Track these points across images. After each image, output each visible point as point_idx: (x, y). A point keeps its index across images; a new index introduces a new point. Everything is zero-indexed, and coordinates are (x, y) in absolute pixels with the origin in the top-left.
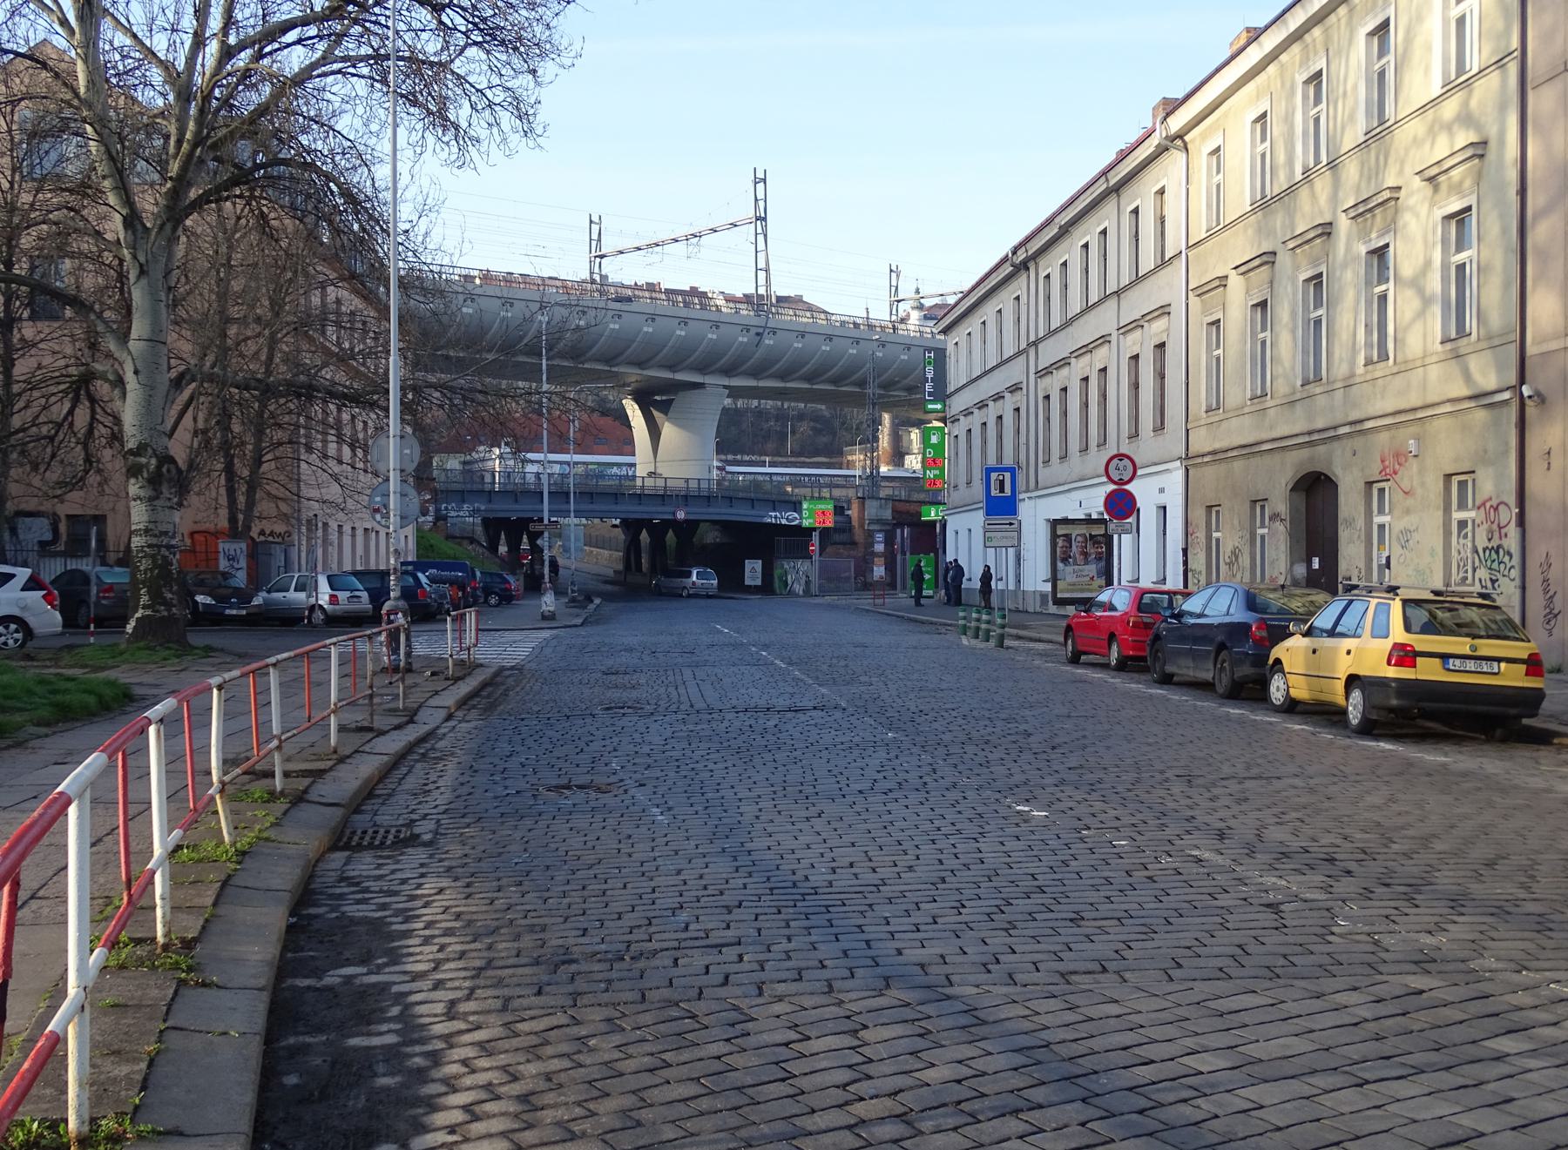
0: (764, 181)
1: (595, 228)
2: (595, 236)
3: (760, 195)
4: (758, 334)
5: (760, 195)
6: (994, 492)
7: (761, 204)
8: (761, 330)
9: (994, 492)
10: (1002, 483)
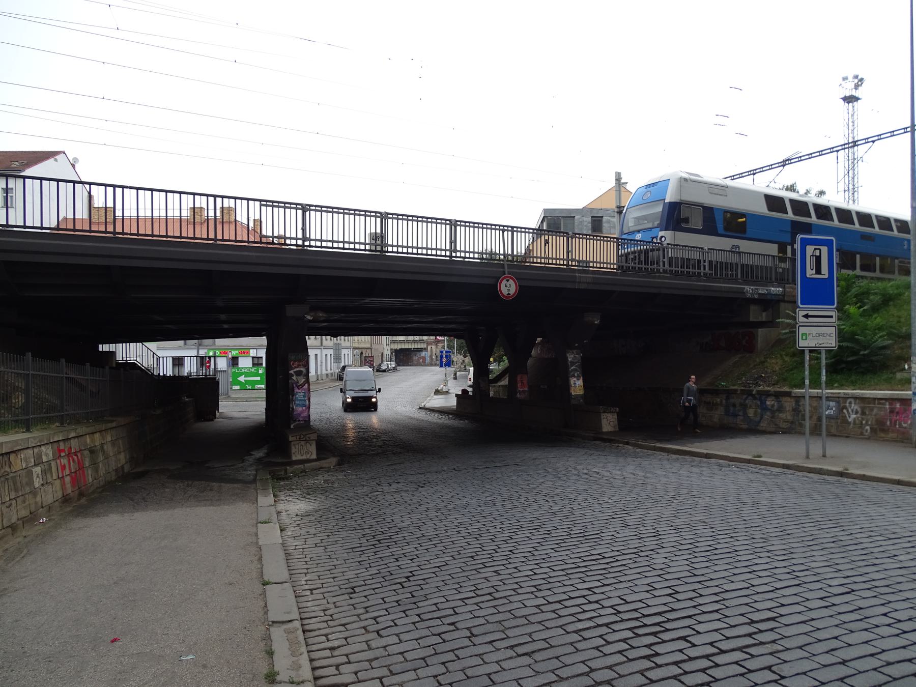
6: (810, 273)
9: (810, 273)
10: (818, 259)
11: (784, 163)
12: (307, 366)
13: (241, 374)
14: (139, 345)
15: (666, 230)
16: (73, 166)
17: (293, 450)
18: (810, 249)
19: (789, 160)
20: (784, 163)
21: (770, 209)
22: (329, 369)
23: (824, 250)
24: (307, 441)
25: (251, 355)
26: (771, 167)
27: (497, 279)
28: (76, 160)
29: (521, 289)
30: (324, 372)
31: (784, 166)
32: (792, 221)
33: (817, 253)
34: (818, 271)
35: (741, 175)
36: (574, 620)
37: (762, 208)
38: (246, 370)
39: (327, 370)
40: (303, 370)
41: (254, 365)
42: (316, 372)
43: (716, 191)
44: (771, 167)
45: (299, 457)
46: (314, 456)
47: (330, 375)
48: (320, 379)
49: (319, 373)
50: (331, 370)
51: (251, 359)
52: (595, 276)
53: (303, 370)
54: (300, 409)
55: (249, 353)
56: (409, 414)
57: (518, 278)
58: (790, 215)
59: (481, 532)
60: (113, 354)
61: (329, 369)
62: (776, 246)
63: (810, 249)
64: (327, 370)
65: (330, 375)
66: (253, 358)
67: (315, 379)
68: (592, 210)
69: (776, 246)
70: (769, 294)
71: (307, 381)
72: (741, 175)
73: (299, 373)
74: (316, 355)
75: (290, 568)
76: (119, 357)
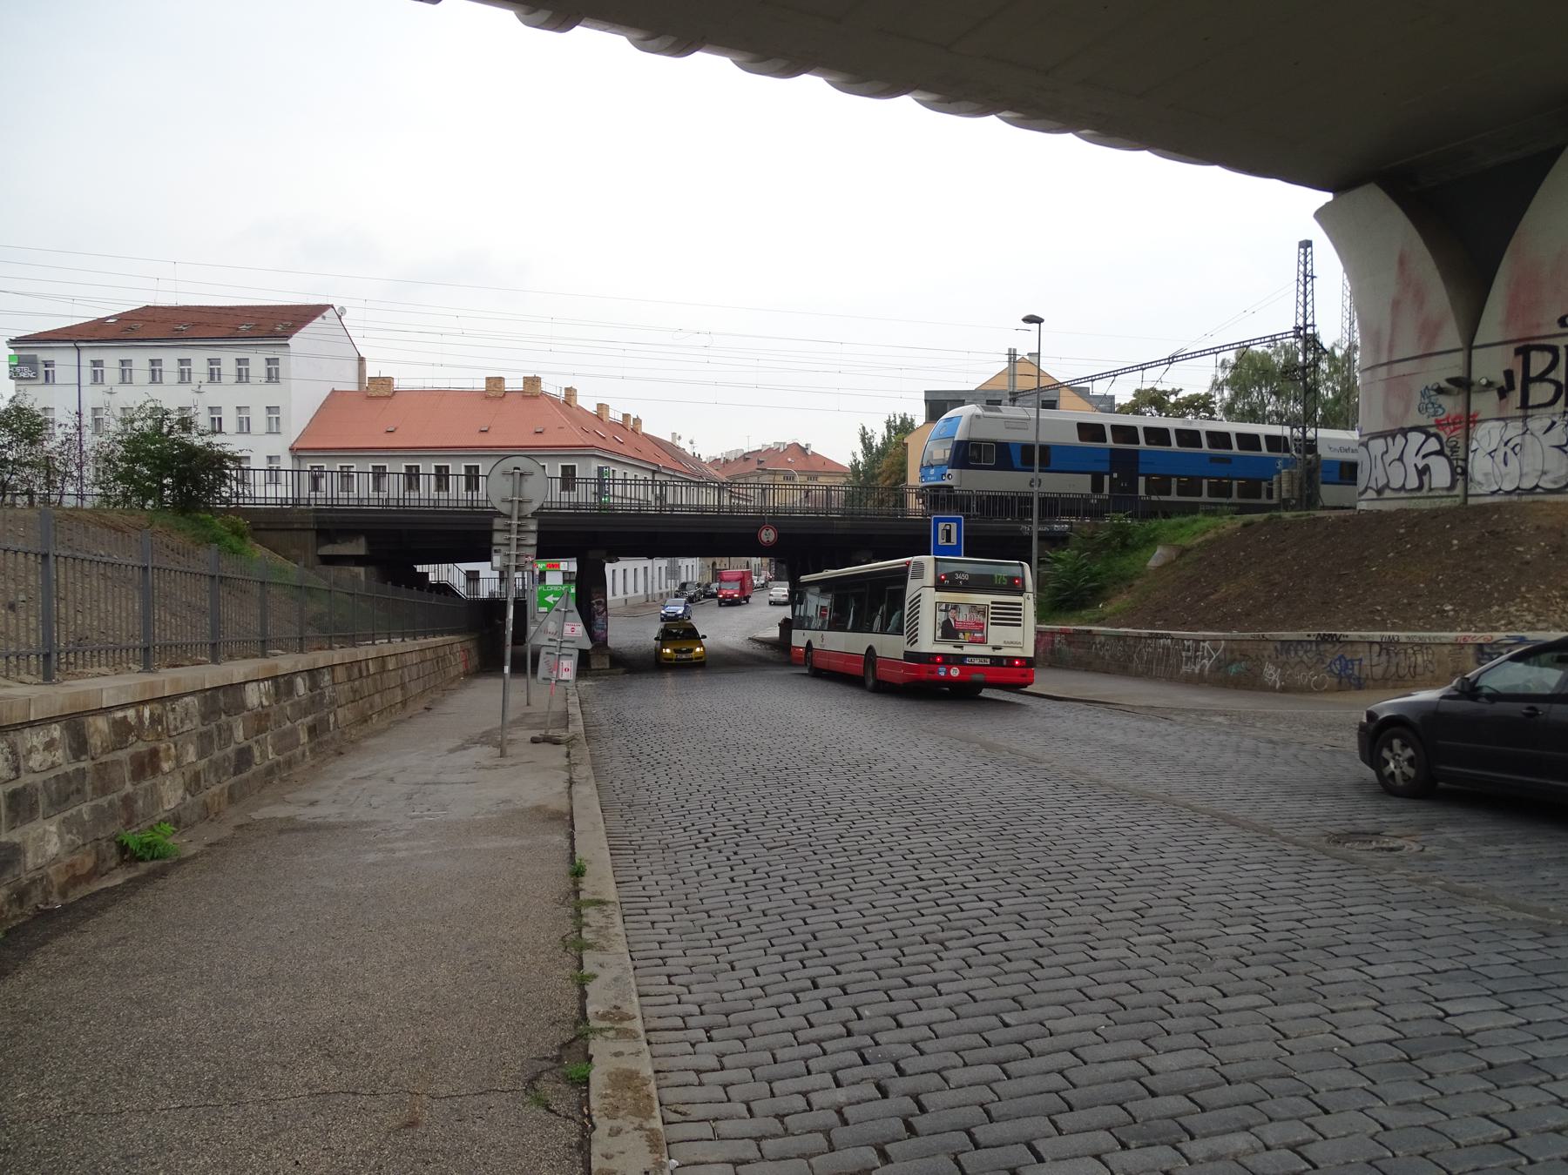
10: (949, 533)
11: (1171, 360)
12: (605, 597)
13: (548, 594)
14: (451, 565)
15: (953, 468)
16: (340, 318)
17: (592, 661)
18: (941, 526)
19: (1173, 357)
20: (1171, 360)
21: (1081, 439)
22: (663, 586)
23: (954, 526)
24: (603, 655)
25: (562, 569)
26: (1157, 363)
27: (759, 528)
28: (342, 308)
29: (780, 536)
30: (657, 590)
31: (1170, 363)
32: (1112, 450)
33: (948, 528)
34: (949, 540)
35: (1101, 376)
36: (1205, 1093)
37: (1073, 438)
38: (556, 589)
39: (660, 588)
40: (603, 600)
41: (565, 581)
42: (646, 591)
43: (1014, 425)
44: (1156, 363)
45: (596, 667)
46: (608, 666)
47: (664, 595)
48: (650, 599)
49: (650, 592)
50: (667, 587)
51: (561, 575)
52: (1037, 461)
53: (603, 600)
54: (600, 631)
55: (558, 566)
56: (734, 646)
57: (777, 528)
58: (1110, 442)
59: (999, 895)
60: (427, 574)
61: (663, 586)
62: (1089, 476)
63: (941, 526)
64: (660, 588)
65: (664, 595)
66: (564, 573)
67: (644, 600)
68: (986, 392)
69: (1089, 476)
70: (1052, 531)
71: (606, 609)
72: (1101, 376)
73: (599, 603)
74: (646, 568)
75: (613, 852)
76: (432, 578)
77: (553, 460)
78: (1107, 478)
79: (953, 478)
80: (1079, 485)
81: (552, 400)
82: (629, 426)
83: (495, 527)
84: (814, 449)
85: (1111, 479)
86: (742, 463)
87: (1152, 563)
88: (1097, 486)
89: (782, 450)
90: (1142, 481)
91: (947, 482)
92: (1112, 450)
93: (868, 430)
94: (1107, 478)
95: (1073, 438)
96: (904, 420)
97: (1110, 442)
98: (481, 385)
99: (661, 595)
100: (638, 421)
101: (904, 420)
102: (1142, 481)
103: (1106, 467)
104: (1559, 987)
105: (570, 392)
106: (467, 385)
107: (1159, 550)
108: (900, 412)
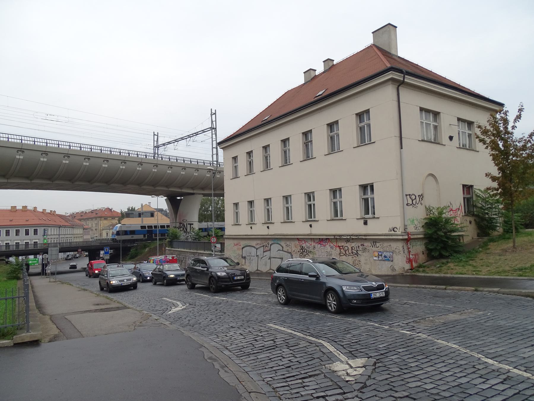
0: (215, 114)
1: (156, 137)
2: (156, 140)
3: (214, 120)
4: (213, 173)
5: (214, 120)
7: (214, 123)
8: (215, 172)
10: (107, 250)
37: (140, 229)
77: (31, 228)
78: (146, 235)
79: (116, 237)
80: (141, 237)
81: (30, 211)
82: (52, 214)
83: (51, 279)
84: (114, 209)
85: (147, 235)
86: (91, 214)
87: (146, 251)
88: (144, 236)
89: (103, 210)
90: (153, 235)
91: (115, 238)
92: (147, 230)
93: (122, 210)
94: (146, 235)
95: (140, 229)
96: (132, 208)
97: (147, 229)
98: (10, 208)
99: (62, 258)
100: (55, 212)
101: (132, 208)
102: (153, 235)
103: (146, 233)
104: (462, 360)
105: (35, 208)
106: (5, 208)
107: (147, 249)
108: (131, 206)
